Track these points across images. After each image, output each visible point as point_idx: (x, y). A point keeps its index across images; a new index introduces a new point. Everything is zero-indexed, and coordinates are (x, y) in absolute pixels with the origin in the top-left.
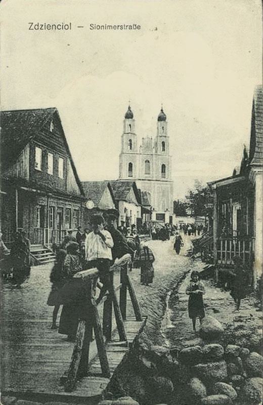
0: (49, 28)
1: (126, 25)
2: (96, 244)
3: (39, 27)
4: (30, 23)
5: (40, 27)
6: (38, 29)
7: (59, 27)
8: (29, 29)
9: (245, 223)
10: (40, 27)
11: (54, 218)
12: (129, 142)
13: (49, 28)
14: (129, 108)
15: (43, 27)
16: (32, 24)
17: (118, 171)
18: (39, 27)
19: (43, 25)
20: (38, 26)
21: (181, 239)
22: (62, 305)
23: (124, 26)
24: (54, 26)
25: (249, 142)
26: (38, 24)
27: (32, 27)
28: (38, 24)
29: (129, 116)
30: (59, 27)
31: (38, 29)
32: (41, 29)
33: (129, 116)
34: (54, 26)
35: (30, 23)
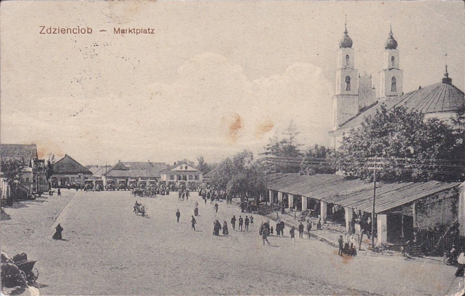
0: (63, 32)
1: (136, 29)
2: (349, 207)
3: (53, 31)
5: (53, 30)
8: (41, 33)
9: (429, 167)
10: (53, 30)
12: (253, 221)
13: (63, 32)
15: (57, 31)
16: (44, 27)
17: (447, 69)
18: (53, 31)
19: (56, 29)
22: (356, 219)
24: (69, 30)
25: (386, 223)
26: (137, 34)
27: (44, 31)
28: (137, 34)
30: (75, 31)
32: (54, 33)
35: (154, 33)
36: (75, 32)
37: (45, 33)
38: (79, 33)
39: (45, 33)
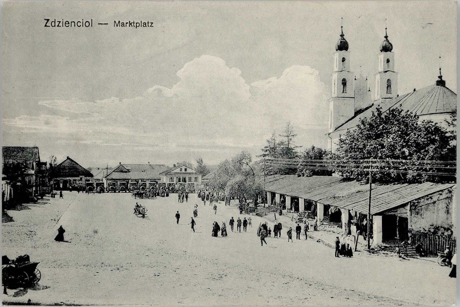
0: (67, 25)
4: (153, 26)
5: (57, 24)
6: (55, 26)
7: (79, 24)
10: (57, 24)
11: (403, 198)
13: (67, 25)
14: (342, 36)
15: (61, 24)
20: (137, 26)
21: (234, 221)
23: (134, 23)
24: (73, 23)
26: (136, 28)
28: (136, 28)
29: (343, 46)
30: (79, 24)
31: (137, 23)
32: (58, 26)
33: (343, 46)
34: (73, 23)
35: (153, 26)
36: (79, 25)
37: (49, 26)
38: (83, 26)
39: (49, 26)
